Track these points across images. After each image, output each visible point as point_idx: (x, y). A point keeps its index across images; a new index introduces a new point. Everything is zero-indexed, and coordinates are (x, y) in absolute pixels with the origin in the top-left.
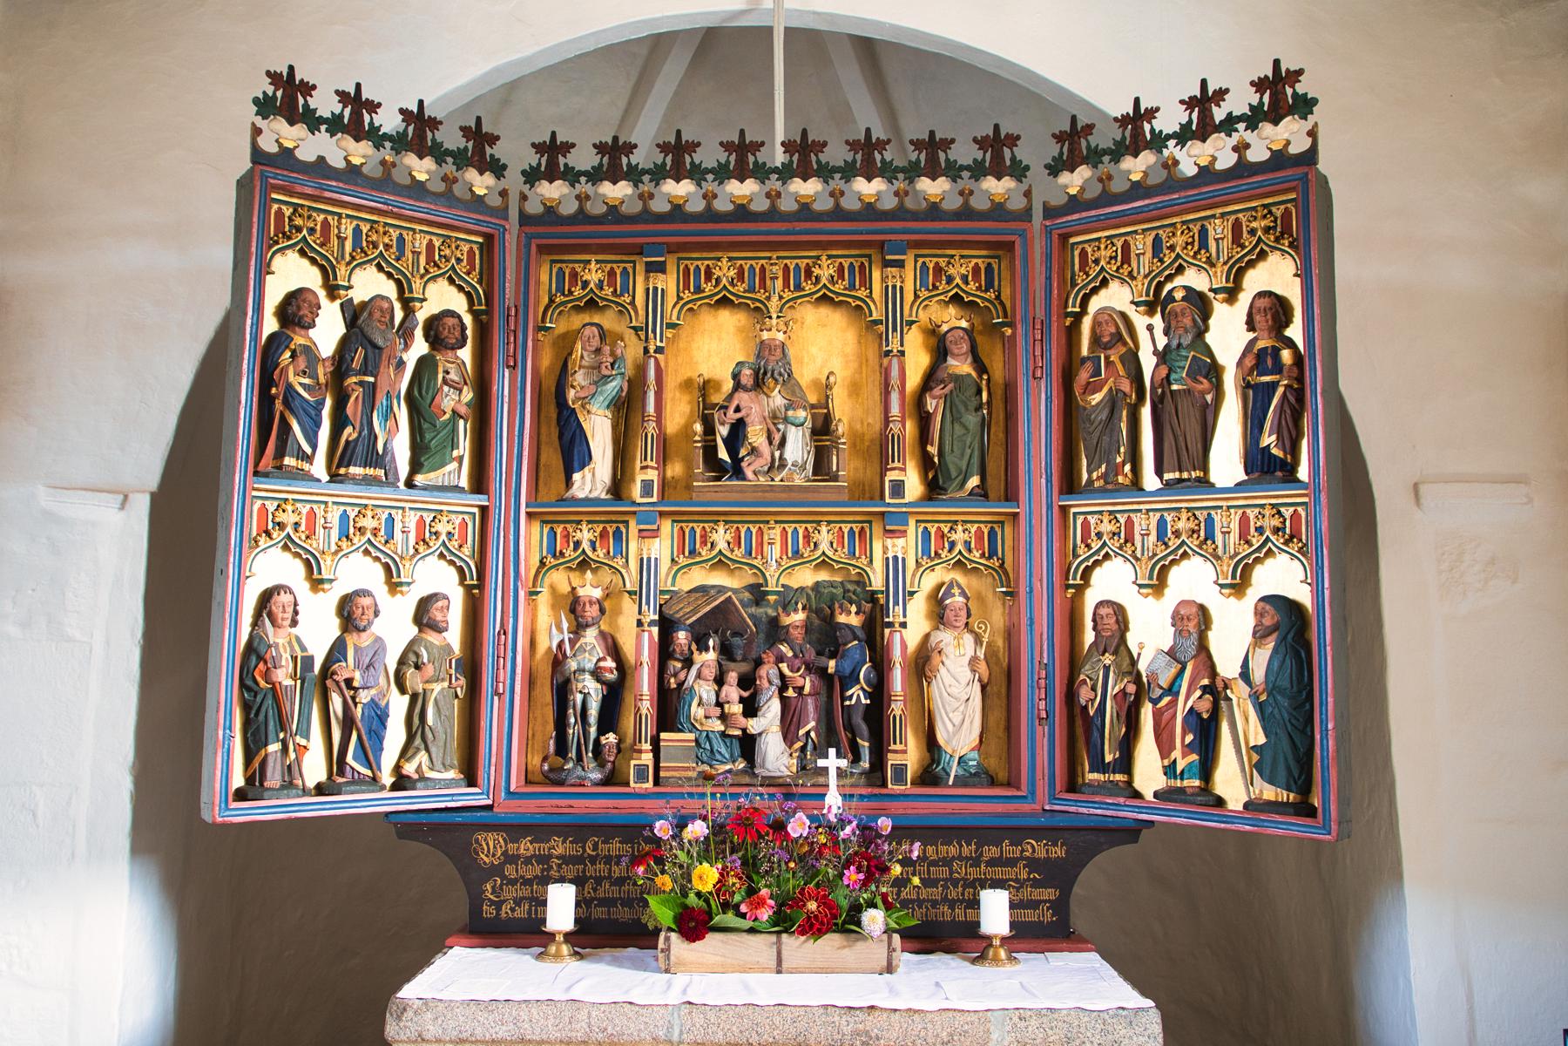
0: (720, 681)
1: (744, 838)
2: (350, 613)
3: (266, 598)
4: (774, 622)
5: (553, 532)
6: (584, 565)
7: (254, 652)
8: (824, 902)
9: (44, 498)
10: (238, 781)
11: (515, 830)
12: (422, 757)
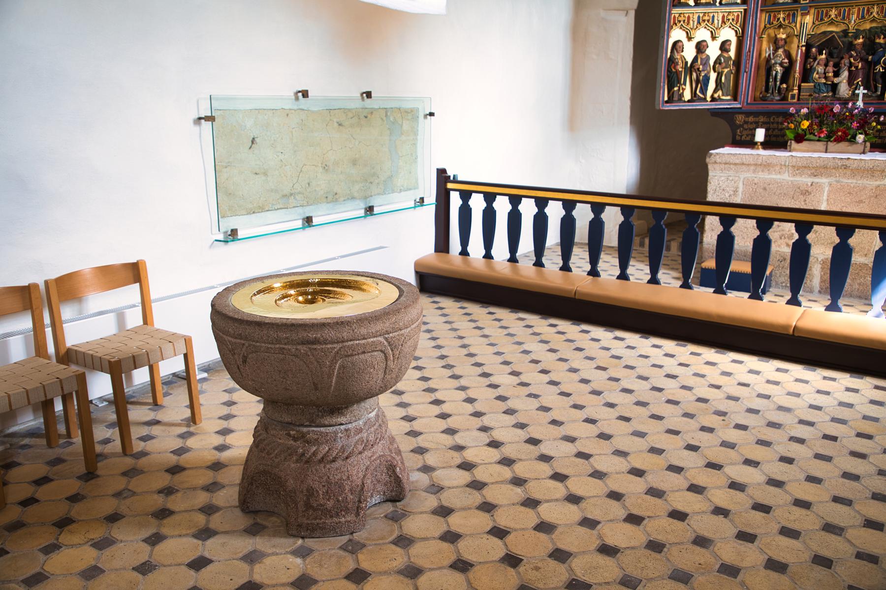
0: (826, 65)
1: (820, 115)
2: (701, 47)
3: (675, 44)
4: (851, 43)
5: (770, 16)
6: (780, 26)
7: (672, 61)
8: (844, 132)
9: (602, 13)
10: (666, 99)
11: (748, 114)
12: (720, 93)
